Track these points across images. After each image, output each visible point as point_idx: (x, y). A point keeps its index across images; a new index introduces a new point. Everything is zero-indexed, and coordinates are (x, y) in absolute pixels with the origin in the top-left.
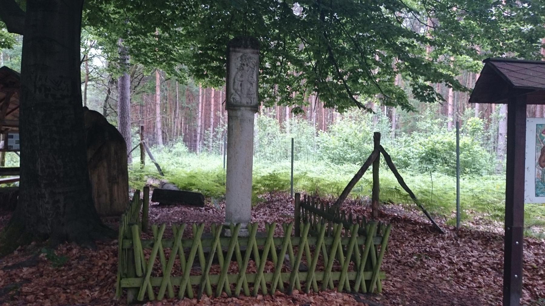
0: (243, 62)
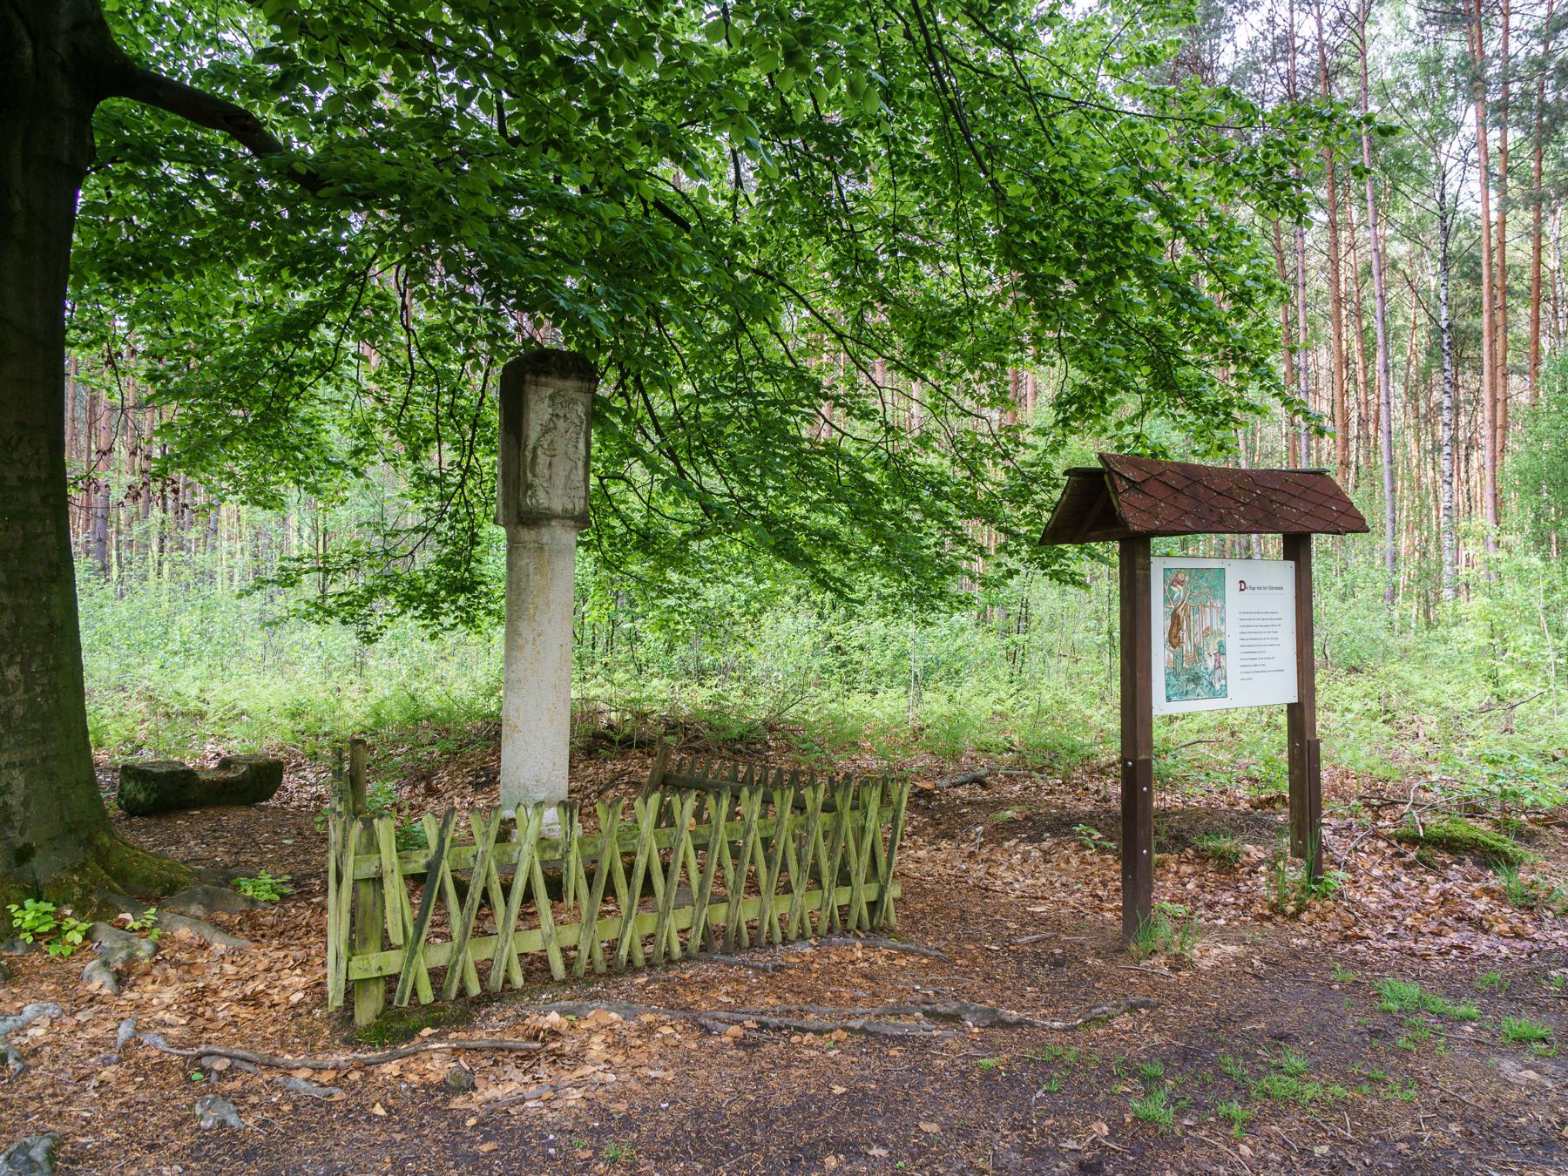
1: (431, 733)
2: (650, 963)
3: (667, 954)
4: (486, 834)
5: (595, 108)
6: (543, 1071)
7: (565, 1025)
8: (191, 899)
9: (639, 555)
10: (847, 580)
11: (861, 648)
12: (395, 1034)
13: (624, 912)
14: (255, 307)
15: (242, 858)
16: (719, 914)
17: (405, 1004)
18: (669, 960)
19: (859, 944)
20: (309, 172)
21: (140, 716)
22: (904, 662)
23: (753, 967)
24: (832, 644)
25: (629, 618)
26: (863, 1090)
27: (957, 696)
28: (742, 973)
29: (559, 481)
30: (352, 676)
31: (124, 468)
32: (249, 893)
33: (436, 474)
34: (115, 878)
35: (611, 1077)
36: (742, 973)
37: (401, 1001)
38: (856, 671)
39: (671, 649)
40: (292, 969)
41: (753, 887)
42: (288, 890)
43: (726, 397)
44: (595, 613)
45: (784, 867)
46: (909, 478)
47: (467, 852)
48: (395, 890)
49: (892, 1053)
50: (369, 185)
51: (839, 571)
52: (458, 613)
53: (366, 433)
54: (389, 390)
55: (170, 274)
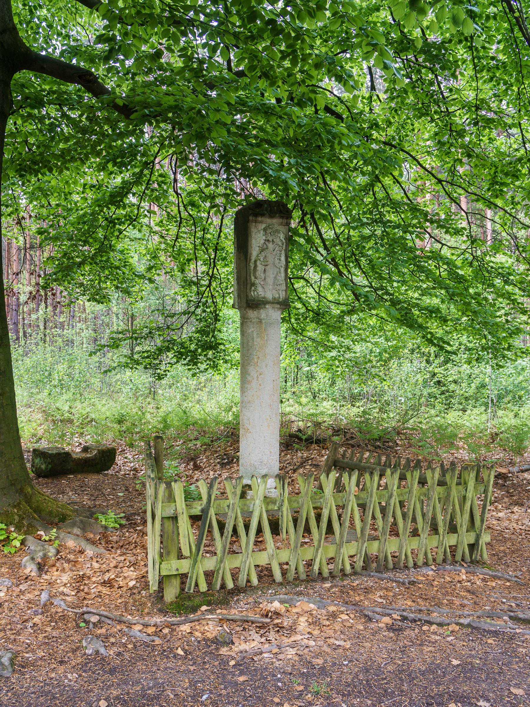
0: (268, 238)
1: (196, 433)
2: (332, 576)
3: (342, 570)
4: (234, 493)
5: (289, 50)
6: (272, 636)
7: (283, 610)
8: (74, 525)
9: (313, 325)
10: (445, 338)
11: (455, 382)
12: (186, 608)
13: (316, 543)
14: (94, 186)
15: (97, 503)
16: (374, 548)
17: (192, 591)
18: (344, 575)
19: (463, 571)
20: (124, 104)
21: (39, 422)
22: (483, 391)
23: (396, 581)
24: (436, 379)
25: (307, 364)
26: (471, 663)
27: (521, 414)
28: (389, 585)
29: (270, 280)
30: (149, 400)
31: (25, 282)
32: (103, 523)
33: (195, 279)
34: (35, 512)
35: (312, 643)
36: (389, 585)
37: (189, 589)
38: (451, 397)
39: (333, 383)
40: (129, 567)
41: (395, 532)
42: (124, 522)
43: (367, 224)
44: (287, 361)
45: (414, 520)
46: (488, 271)
47: (224, 504)
48: (184, 523)
49: (490, 641)
50: (158, 109)
51: (439, 333)
52: (208, 362)
53: (155, 257)
54: (167, 230)
55: (50, 170)
